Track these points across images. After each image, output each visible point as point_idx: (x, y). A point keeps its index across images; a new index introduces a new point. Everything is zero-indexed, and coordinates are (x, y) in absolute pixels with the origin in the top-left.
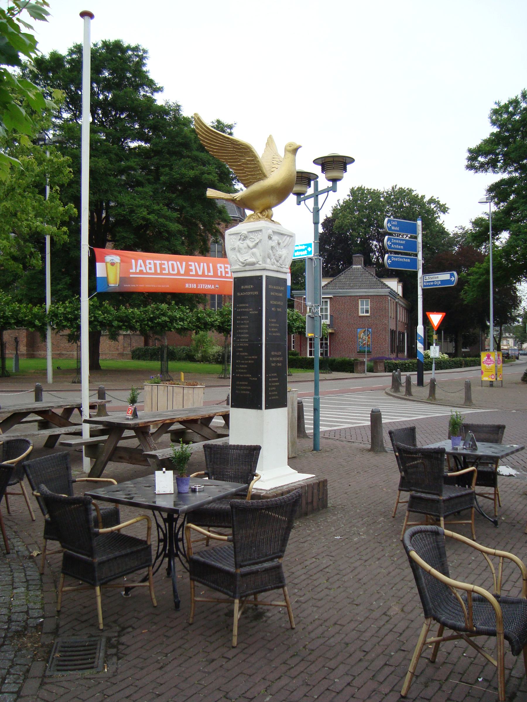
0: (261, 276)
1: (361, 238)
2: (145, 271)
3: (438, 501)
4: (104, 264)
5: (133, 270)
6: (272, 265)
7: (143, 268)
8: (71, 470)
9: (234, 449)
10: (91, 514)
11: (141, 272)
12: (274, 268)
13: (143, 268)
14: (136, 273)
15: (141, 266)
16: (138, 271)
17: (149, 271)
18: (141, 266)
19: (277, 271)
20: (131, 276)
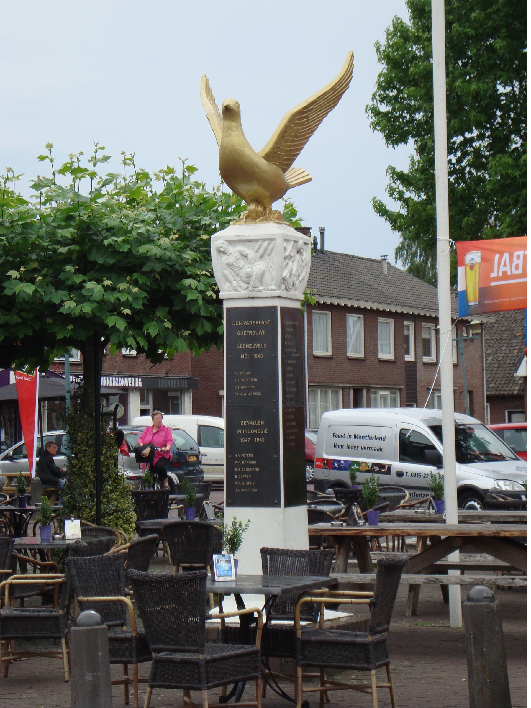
0: (275, 308)
1: (487, 158)
2: (509, 273)
3: (195, 664)
4: (464, 267)
5: (493, 275)
6: (236, 290)
7: (507, 268)
8: (400, 561)
9: (279, 555)
10: (84, 546)
11: (505, 276)
12: (243, 293)
13: (507, 268)
14: (497, 279)
15: (505, 265)
16: (500, 274)
17: (515, 272)
18: (505, 265)
19: (253, 298)
20: (492, 284)
